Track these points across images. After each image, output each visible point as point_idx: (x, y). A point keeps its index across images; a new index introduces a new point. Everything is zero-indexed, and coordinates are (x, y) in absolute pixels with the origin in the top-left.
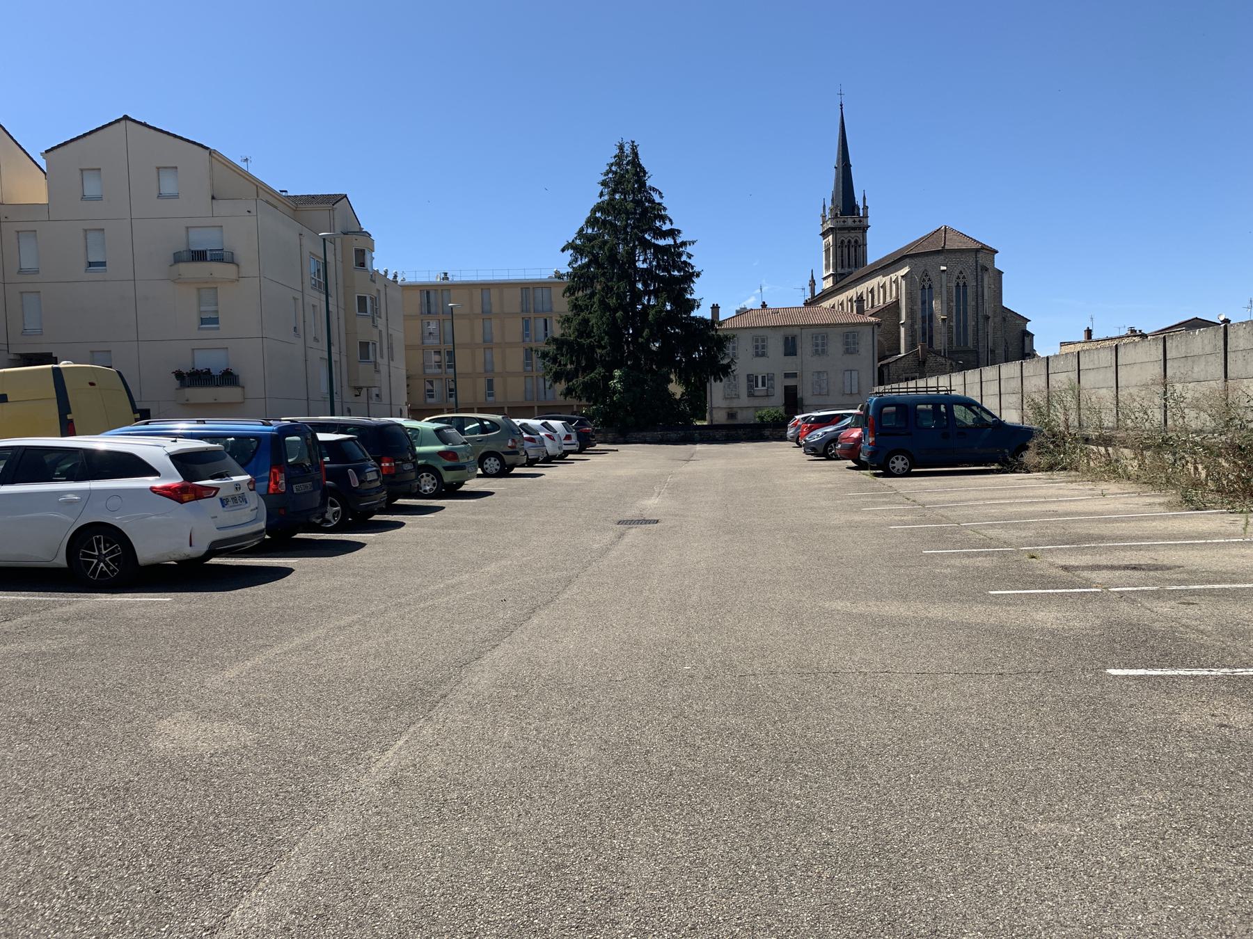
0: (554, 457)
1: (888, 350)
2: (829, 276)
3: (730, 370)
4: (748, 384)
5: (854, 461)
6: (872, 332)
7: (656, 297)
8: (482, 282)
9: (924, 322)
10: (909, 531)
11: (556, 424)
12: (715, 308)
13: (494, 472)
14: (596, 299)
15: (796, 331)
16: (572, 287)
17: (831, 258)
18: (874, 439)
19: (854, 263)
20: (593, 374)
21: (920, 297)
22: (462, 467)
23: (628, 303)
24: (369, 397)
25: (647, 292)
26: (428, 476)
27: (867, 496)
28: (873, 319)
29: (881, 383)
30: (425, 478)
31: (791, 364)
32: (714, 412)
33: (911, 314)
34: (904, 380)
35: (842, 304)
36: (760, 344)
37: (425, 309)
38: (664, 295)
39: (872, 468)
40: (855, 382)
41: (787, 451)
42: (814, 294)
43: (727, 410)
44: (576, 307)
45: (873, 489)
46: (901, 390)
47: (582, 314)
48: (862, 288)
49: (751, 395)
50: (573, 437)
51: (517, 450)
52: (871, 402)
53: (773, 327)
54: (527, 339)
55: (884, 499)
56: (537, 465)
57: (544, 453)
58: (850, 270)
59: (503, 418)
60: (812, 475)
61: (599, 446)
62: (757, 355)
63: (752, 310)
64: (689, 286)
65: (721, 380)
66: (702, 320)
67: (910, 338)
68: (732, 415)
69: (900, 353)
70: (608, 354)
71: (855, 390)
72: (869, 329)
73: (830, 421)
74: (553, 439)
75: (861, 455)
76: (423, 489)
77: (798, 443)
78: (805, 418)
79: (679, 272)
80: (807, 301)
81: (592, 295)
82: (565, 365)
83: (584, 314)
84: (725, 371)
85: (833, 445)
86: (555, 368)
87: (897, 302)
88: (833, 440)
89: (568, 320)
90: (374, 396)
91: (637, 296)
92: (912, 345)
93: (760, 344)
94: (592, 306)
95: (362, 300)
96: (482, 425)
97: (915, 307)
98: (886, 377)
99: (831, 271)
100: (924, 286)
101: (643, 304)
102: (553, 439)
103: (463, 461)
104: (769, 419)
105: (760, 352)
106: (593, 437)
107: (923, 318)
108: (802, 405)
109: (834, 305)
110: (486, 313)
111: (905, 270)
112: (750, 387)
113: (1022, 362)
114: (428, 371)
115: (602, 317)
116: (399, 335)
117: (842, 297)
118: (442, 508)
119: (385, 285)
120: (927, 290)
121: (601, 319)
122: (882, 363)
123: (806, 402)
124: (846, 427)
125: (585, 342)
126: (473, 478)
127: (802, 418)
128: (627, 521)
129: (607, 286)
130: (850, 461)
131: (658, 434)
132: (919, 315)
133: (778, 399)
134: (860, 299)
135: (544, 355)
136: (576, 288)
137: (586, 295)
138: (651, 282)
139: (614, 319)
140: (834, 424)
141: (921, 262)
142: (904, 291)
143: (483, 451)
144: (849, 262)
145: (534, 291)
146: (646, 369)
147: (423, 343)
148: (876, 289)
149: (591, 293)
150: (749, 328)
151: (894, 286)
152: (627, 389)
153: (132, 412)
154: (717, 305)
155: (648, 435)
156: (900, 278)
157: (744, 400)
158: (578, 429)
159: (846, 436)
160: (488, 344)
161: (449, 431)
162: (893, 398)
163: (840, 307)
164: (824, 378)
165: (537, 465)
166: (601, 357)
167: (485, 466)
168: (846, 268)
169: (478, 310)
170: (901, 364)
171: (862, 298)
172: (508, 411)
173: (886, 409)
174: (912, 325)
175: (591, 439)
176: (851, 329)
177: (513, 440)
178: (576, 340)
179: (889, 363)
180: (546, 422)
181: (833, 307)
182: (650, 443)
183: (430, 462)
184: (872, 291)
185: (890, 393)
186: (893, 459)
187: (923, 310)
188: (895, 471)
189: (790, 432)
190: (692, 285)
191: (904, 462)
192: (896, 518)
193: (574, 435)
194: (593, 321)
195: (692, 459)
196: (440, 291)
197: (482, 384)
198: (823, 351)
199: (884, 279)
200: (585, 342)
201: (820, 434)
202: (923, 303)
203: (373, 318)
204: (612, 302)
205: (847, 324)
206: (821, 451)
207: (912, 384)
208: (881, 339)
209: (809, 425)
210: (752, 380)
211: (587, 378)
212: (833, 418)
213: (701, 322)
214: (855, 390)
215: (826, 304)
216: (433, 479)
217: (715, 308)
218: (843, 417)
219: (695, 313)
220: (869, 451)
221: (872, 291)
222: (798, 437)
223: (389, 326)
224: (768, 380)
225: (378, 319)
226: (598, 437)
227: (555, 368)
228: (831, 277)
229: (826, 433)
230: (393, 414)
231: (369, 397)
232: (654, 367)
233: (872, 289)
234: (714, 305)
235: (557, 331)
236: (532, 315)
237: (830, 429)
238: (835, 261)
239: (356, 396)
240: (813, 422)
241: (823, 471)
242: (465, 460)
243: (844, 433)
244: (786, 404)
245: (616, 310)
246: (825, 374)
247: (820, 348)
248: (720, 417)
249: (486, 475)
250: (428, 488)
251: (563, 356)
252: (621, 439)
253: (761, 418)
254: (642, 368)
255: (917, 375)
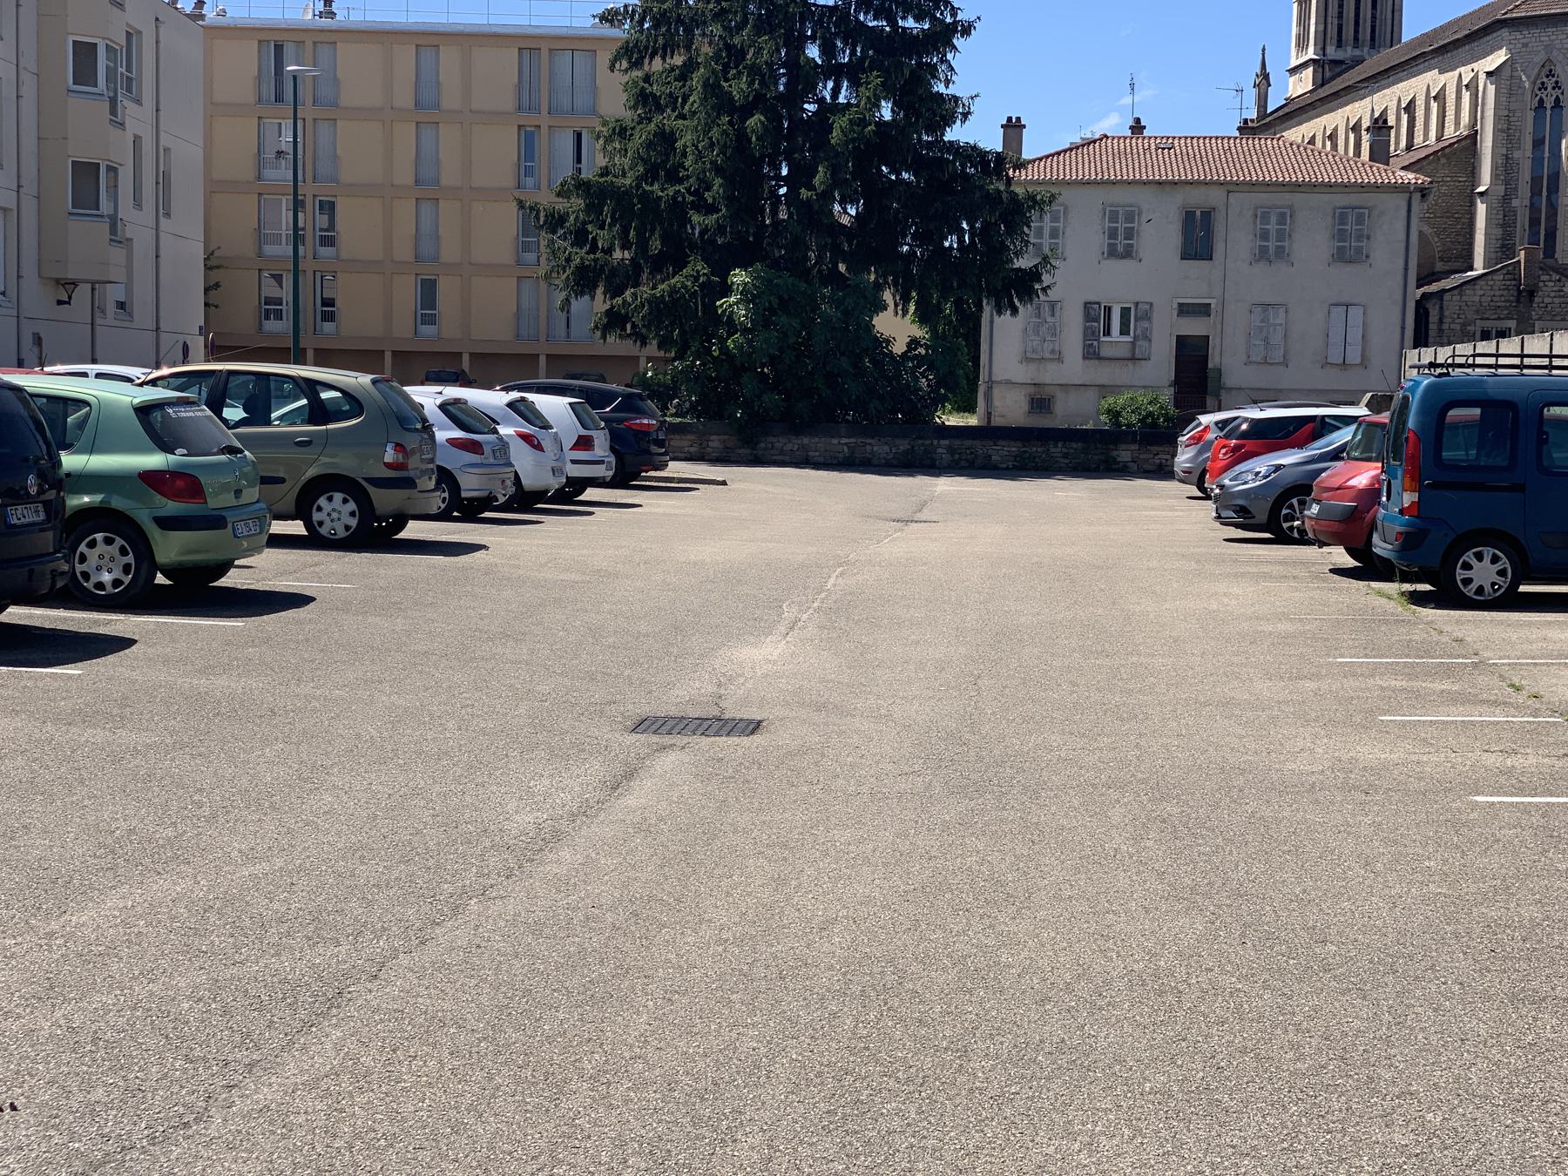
0: (540, 495)
1: (1441, 259)
2: (1304, 65)
3: (1037, 286)
4: (1086, 329)
5: (1352, 552)
6: (1405, 208)
7: (855, 84)
8: (422, 28)
9: (1535, 191)
10: (1536, 819)
11: (553, 406)
12: (1013, 128)
13: (342, 534)
14: (696, 80)
15: (1216, 197)
16: (636, 45)
17: (1313, 21)
18: (1415, 497)
19: (1368, 37)
20: (677, 278)
21: (1530, 128)
22: (215, 522)
23: (780, 97)
24: (96, 309)
25: (834, 71)
26: (109, 541)
27: (1392, 670)
28: (1410, 177)
29: (1421, 341)
30: (101, 548)
31: (1196, 281)
32: (996, 392)
33: (1505, 168)
34: (1478, 335)
35: (1333, 137)
36: (1121, 226)
37: (269, 91)
38: (875, 79)
39: (1405, 578)
40: (1355, 335)
41: (1172, 509)
42: (1266, 108)
43: (1032, 389)
44: (644, 99)
45: (1409, 648)
46: (1502, 361)
47: (658, 118)
48: (1387, 99)
49: (1091, 353)
50: (596, 442)
51: (411, 474)
52: (1413, 390)
53: (1159, 183)
54: (530, 181)
55: (1446, 686)
56: (487, 514)
57: (509, 483)
58: (1357, 52)
59: (374, 382)
60: (1236, 590)
61: (676, 469)
62: (1112, 253)
63: (1107, 137)
64: (943, 60)
65: (1015, 311)
66: (972, 154)
67: (1500, 231)
68: (1040, 403)
69: (1471, 269)
70: (721, 229)
71: (1354, 356)
72: (1400, 201)
73: (1289, 434)
74: (538, 447)
75: (1376, 538)
76: (94, 579)
77: (1201, 487)
78: (1225, 422)
79: (918, 19)
80: (1246, 121)
81: (685, 73)
82: (609, 251)
83: (668, 120)
84: (1024, 286)
85: (1295, 501)
86: (580, 255)
87: (1471, 141)
88: (1299, 489)
89: (622, 132)
90: (111, 308)
91: (804, 78)
92: (1502, 248)
93: (1121, 226)
94: (685, 99)
95: (85, 53)
96: (316, 404)
97: (1517, 154)
98: (1433, 327)
99: (1311, 54)
100: (1541, 99)
101: (821, 101)
102: (538, 447)
103: (217, 501)
104: (1134, 419)
105: (1121, 246)
106: (660, 443)
107: (1536, 182)
108: (1220, 387)
109: (1314, 136)
110: (426, 107)
111: (1498, 58)
112: (1090, 336)
113: (1552, 335)
114: (269, 250)
115: (710, 129)
116: (187, 152)
117: (1336, 119)
118: (123, 643)
119: (157, 19)
120: (1549, 112)
121: (706, 132)
122: (1426, 289)
123: (1229, 380)
124: (1336, 455)
125: (660, 191)
126: (258, 550)
127: (1217, 423)
128: (667, 719)
129: (728, 47)
130: (1341, 550)
131: (841, 444)
132: (1525, 175)
133: (1159, 369)
134: (1380, 126)
135: (555, 221)
136: (646, 48)
137: (673, 69)
138: (846, 44)
139: (742, 137)
140: (1300, 445)
141: (1538, 39)
142: (1490, 113)
143: (311, 472)
144: (1356, 31)
145: (550, 55)
146: (820, 271)
147: (259, 178)
148: (1420, 103)
149: (685, 63)
150: (1096, 183)
151: (1466, 96)
152: (763, 320)
153: (1080, 356)
154: (1018, 119)
155: (816, 444)
156: (1482, 77)
157: (1073, 368)
158: (620, 421)
159: (1336, 482)
160: (426, 187)
161: (186, 413)
162: (1479, 382)
163: (1328, 143)
164: (1278, 321)
165: (487, 514)
166: (702, 233)
167: (316, 516)
168: (1349, 49)
169: (405, 98)
170: (1474, 296)
171: (1385, 121)
172: (471, 364)
173: (1454, 413)
174: (1506, 199)
175: (655, 449)
176: (1353, 199)
177: (399, 447)
178: (638, 186)
179: (1444, 291)
180: (523, 399)
181: (1312, 141)
182: (817, 466)
183: (118, 503)
184: (1410, 108)
185: (1469, 366)
186: (1469, 557)
187: (1537, 162)
188: (1470, 591)
189: (1184, 457)
190: (949, 56)
191: (1498, 567)
192: (1491, 760)
193: (601, 440)
194: (686, 140)
195: (919, 516)
196: (309, 45)
197: (406, 293)
198: (1281, 253)
199: (1443, 78)
200: (660, 191)
201: (1263, 470)
202: (1538, 143)
203: (113, 102)
204: (738, 88)
205: (1346, 187)
206: (1262, 516)
207: (1510, 345)
208: (1427, 230)
209: (1233, 442)
210: (1096, 316)
211: (661, 287)
212: (1296, 430)
213: (969, 157)
214: (1354, 356)
215: (1296, 134)
216: (123, 552)
217: (1013, 128)
218: (1322, 427)
219: (956, 133)
220: (1402, 529)
221: (1410, 108)
222: (1204, 472)
223: (162, 128)
224: (1136, 320)
225: (127, 103)
226: (677, 442)
227: (580, 255)
228: (1311, 69)
229: (1278, 468)
230: (98, 356)
231: (96, 309)
232: (842, 268)
233: (1412, 103)
234: (1010, 119)
235: (595, 160)
236: (544, 120)
237: (1289, 458)
238: (1321, 27)
239: (60, 302)
240: (1244, 435)
241: (1267, 576)
242: (228, 500)
243: (1335, 473)
244: (1178, 382)
245: (747, 111)
246: (1282, 311)
247: (1272, 245)
248: (1010, 408)
249: (314, 540)
250: (106, 577)
251: (602, 228)
252: (745, 451)
253: (1115, 414)
254: (810, 270)
255: (1512, 324)
